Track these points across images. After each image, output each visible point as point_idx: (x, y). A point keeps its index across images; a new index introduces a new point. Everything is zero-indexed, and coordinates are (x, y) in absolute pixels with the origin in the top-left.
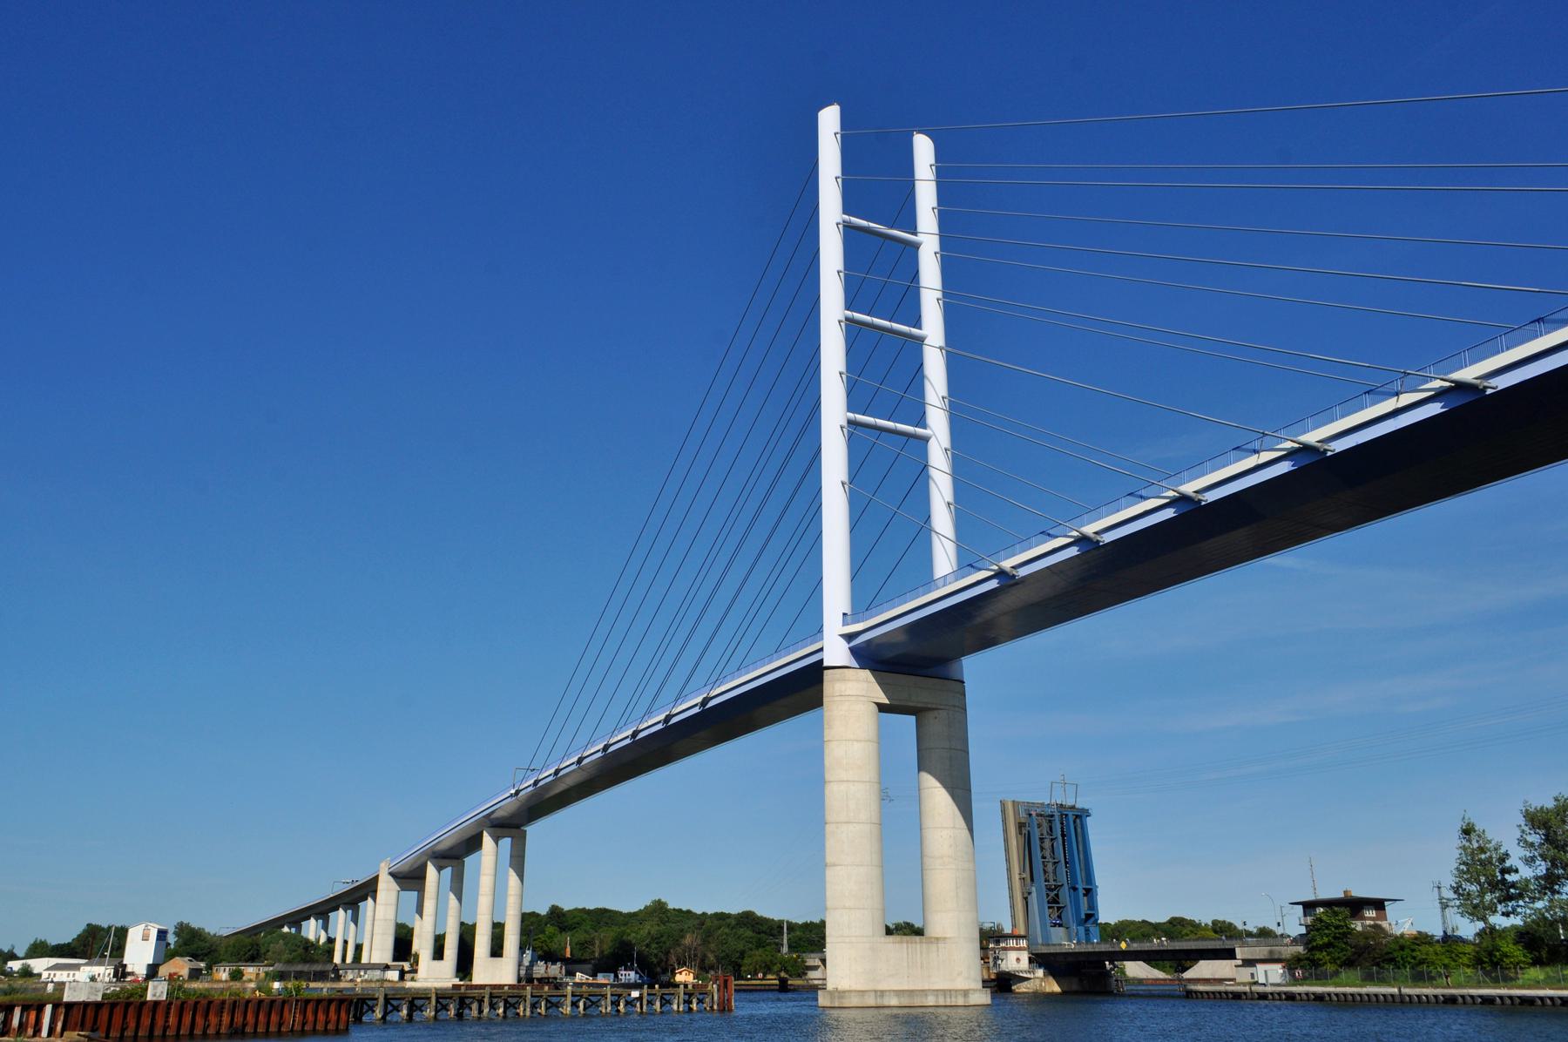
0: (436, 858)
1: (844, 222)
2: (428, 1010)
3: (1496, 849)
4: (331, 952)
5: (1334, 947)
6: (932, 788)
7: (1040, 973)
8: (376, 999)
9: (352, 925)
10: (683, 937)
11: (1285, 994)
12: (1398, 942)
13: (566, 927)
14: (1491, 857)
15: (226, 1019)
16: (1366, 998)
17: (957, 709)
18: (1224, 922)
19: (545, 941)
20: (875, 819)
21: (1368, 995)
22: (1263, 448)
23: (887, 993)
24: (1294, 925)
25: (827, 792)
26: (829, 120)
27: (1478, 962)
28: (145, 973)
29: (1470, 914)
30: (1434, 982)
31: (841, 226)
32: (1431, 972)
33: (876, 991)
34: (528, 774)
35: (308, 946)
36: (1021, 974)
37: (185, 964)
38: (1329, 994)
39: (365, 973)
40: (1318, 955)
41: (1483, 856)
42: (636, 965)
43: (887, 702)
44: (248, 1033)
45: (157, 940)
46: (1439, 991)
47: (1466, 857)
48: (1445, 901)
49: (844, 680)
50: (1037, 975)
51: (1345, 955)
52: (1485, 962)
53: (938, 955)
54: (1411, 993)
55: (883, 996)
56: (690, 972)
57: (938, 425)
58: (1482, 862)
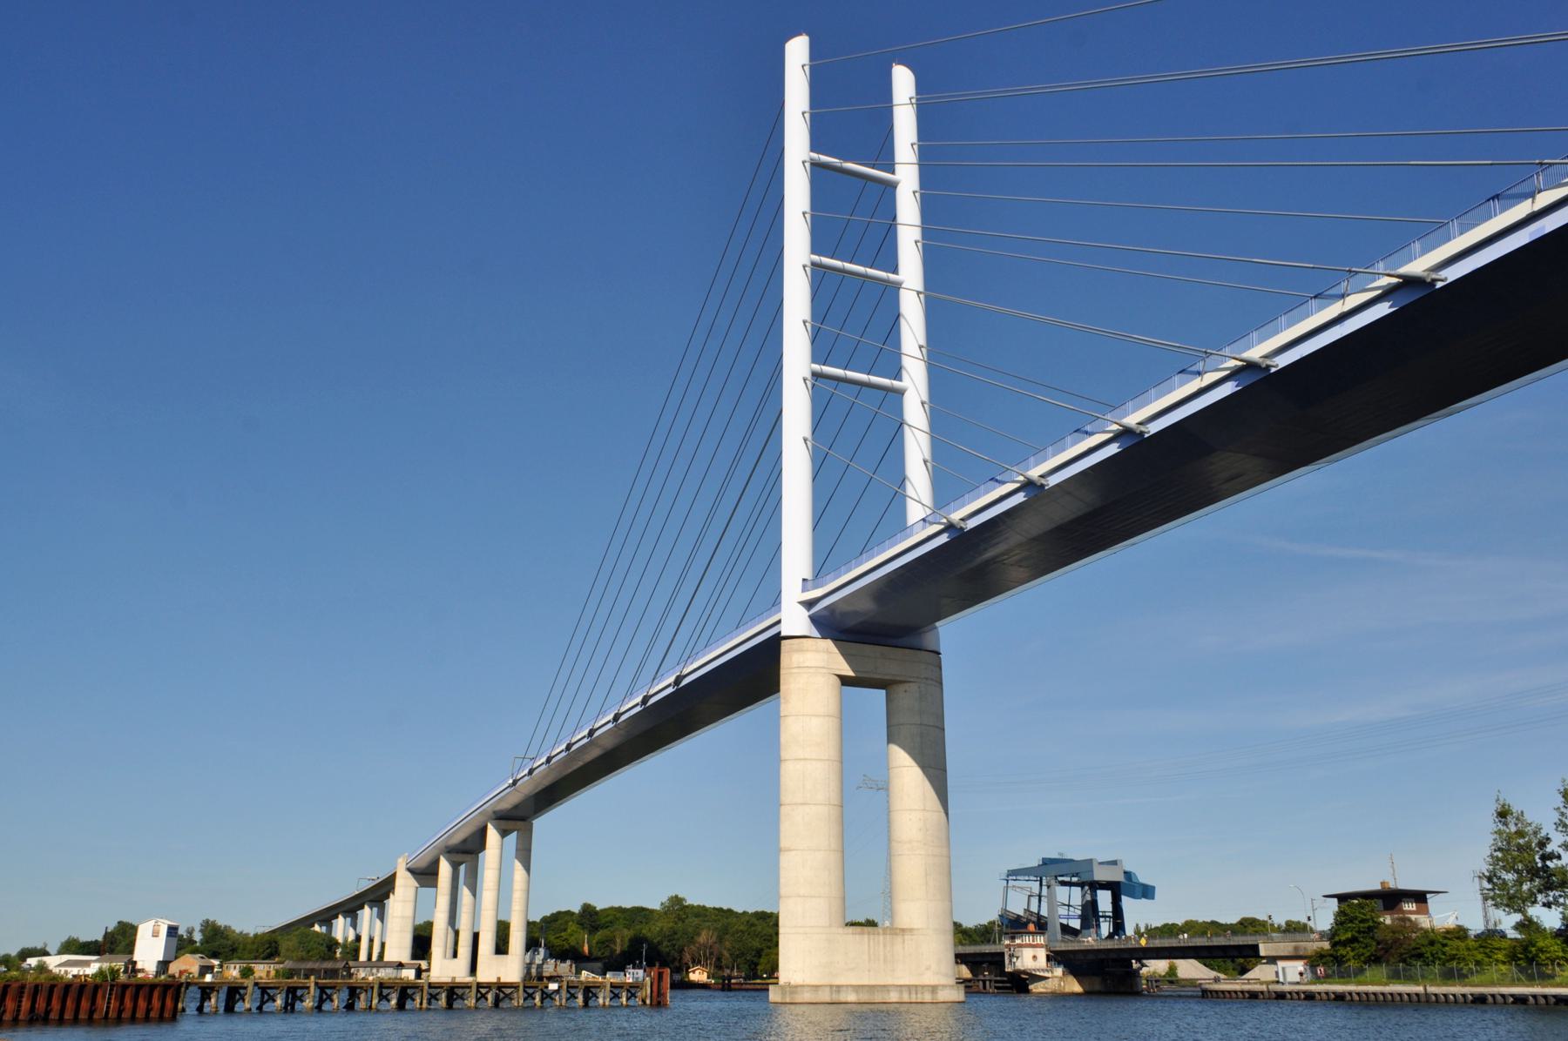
0: (449, 852)
1: (811, 159)
2: (307, 1001)
3: (1535, 833)
4: (356, 951)
5: (1358, 942)
6: (900, 767)
7: (1059, 971)
8: (245, 988)
9: (378, 922)
10: (699, 934)
11: (1304, 993)
12: (1427, 937)
13: (599, 925)
14: (1529, 842)
15: (26, 1004)
16: (1390, 997)
17: (930, 682)
18: (1299, 922)
20: (835, 799)
21: (1391, 994)
22: (1206, 369)
23: (844, 989)
24: (1324, 919)
26: (797, 51)
27: (1513, 957)
28: (155, 969)
29: (1507, 905)
30: (1466, 980)
31: (807, 165)
32: (1462, 969)
33: (831, 986)
34: (524, 763)
35: (332, 944)
36: (1038, 973)
37: (196, 961)
38: (1350, 994)
39: (378, 971)
40: (1342, 951)
41: (1521, 841)
42: (644, 963)
43: (851, 673)
44: (21, 1020)
45: (168, 936)
46: (1467, 990)
47: (1502, 842)
48: (1486, 892)
51: (1368, 951)
52: (1520, 959)
53: (904, 948)
54: (1437, 992)
55: (839, 991)
57: (914, 380)
58: (1520, 848)
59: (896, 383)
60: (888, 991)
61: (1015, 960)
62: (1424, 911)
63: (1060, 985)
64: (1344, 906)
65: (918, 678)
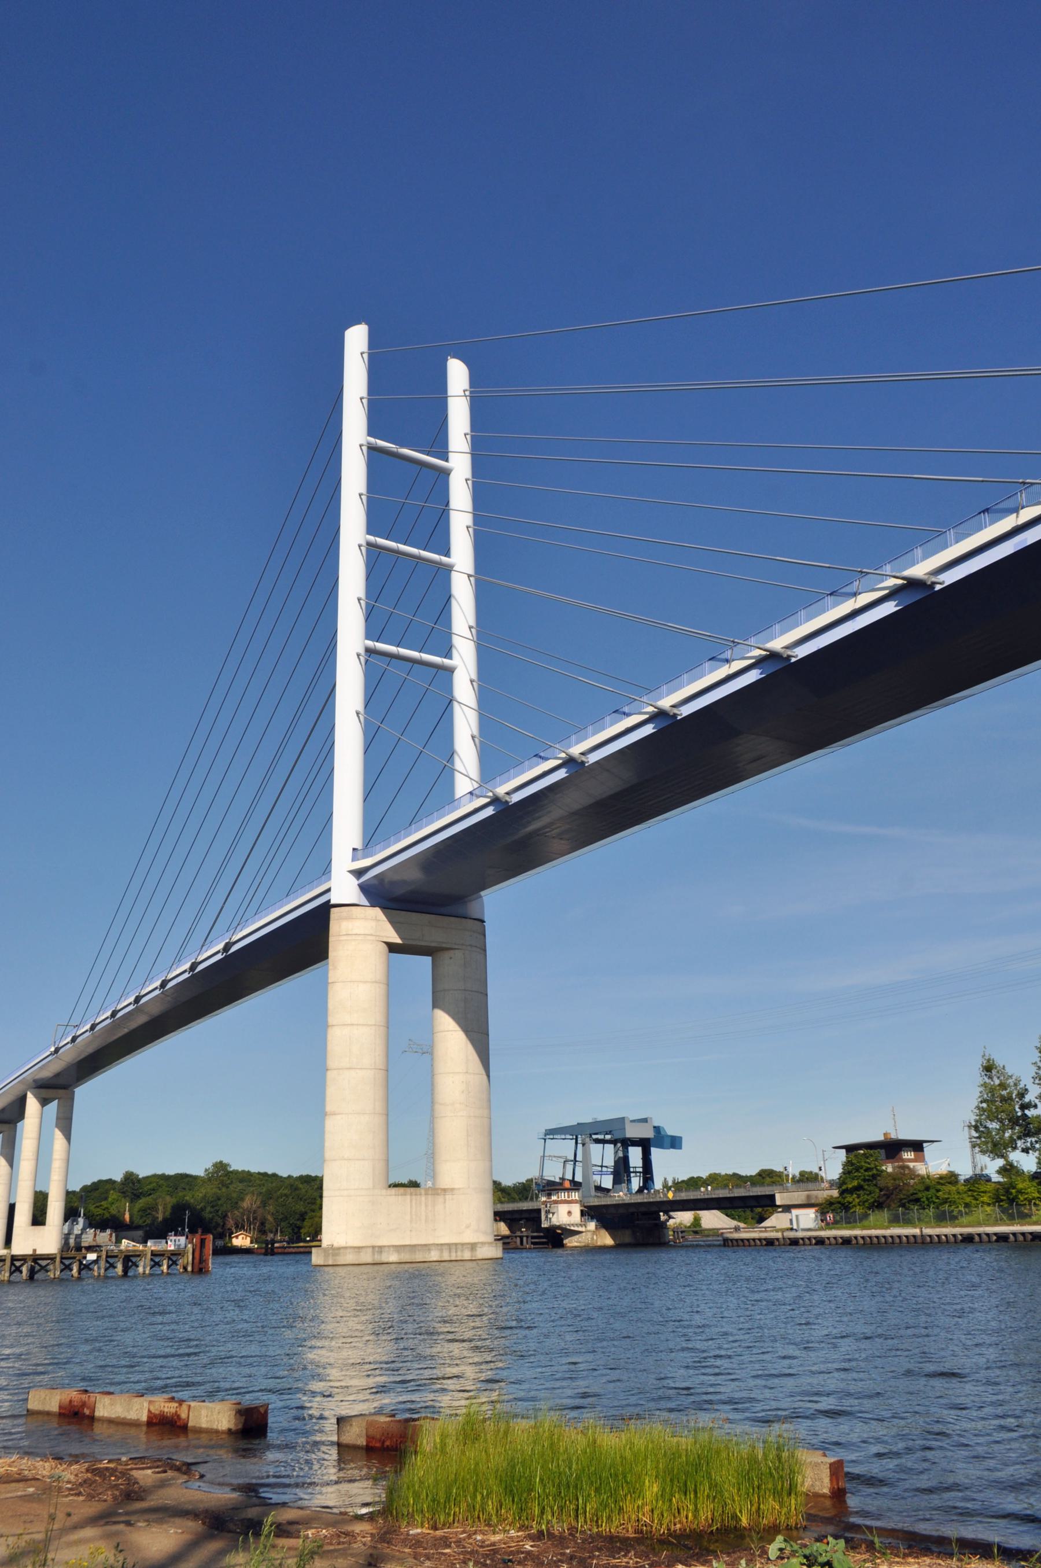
7: (592, 1225)
10: (242, 1199)
11: (815, 1238)
13: (141, 1193)
14: (1011, 1093)
19: (107, 1208)
21: (892, 1237)
24: (833, 1169)
25: (329, 1037)
27: (997, 1200)
30: (957, 1222)
31: (365, 448)
32: (953, 1211)
33: (373, 1247)
36: (572, 1228)
43: (399, 941)
46: (958, 1230)
49: (349, 918)
50: (589, 1228)
52: (1002, 1201)
55: (381, 1252)
56: (247, 1236)
59: (446, 661)
60: (429, 1250)
61: (550, 1216)
62: (921, 1159)
63: (592, 1239)
64: (852, 1156)
65: (462, 945)
